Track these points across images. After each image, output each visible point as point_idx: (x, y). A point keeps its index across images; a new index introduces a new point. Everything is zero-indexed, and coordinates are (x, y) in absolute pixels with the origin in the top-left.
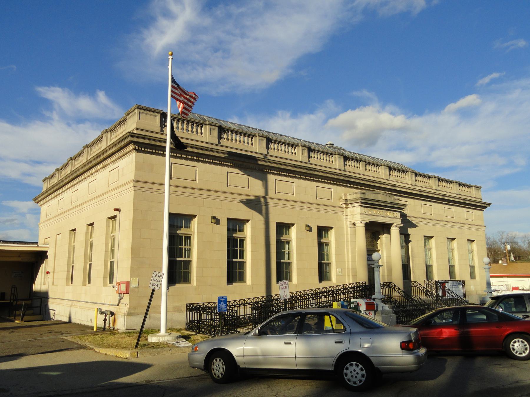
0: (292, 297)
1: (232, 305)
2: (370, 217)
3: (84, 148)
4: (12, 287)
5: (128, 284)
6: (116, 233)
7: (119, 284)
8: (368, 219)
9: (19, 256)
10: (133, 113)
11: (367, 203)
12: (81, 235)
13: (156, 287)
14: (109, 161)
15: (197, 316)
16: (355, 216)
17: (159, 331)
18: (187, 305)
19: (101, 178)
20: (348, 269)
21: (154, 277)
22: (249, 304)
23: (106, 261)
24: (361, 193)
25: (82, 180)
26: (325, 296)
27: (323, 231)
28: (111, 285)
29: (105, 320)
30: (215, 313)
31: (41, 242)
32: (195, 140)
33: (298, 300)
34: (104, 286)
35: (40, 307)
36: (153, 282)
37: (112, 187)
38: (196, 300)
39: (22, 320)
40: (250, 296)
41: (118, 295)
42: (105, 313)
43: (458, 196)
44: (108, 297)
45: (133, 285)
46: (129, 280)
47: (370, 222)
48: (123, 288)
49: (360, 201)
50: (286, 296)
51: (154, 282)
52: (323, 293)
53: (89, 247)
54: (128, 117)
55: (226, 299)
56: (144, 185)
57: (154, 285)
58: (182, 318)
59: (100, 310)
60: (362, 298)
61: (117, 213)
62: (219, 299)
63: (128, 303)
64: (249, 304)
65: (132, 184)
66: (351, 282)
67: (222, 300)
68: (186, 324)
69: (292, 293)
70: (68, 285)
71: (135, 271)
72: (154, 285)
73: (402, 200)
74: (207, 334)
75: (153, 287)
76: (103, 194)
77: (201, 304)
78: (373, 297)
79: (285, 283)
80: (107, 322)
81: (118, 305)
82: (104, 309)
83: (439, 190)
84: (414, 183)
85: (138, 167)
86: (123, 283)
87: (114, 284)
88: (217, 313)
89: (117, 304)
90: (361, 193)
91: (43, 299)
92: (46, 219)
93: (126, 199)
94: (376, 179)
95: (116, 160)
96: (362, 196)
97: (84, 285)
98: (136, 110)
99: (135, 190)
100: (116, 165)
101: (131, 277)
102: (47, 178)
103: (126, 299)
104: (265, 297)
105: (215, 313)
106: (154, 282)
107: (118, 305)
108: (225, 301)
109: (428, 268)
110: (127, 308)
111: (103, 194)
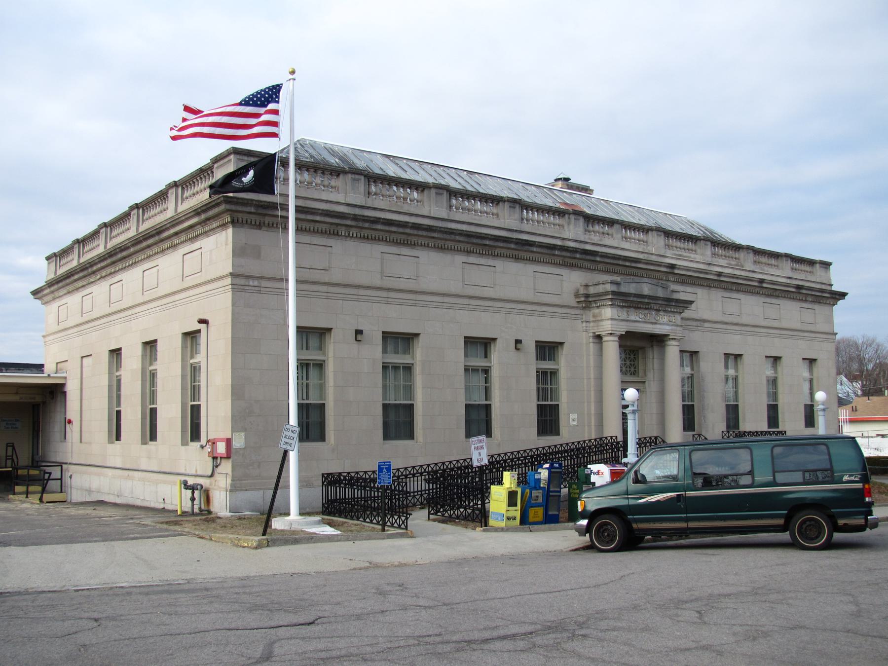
0: (491, 463)
1: (402, 475)
2: (628, 323)
3: (132, 208)
4: (7, 446)
5: (229, 442)
6: (200, 358)
7: (214, 443)
8: (623, 328)
9: (17, 393)
10: (226, 160)
11: (625, 301)
12: (132, 361)
13: (289, 448)
14: (183, 237)
15: (338, 492)
16: (601, 323)
17: (288, 514)
18: (323, 475)
19: (167, 268)
20: (589, 414)
21: (286, 433)
22: (421, 474)
23: (184, 405)
24: (612, 283)
25: (130, 265)
26: (565, 458)
27: (547, 350)
28: (196, 445)
29: (193, 499)
30: (371, 488)
31: (49, 368)
32: (327, 201)
33: (502, 467)
34: (182, 445)
35: (61, 479)
36: (284, 440)
37: (189, 282)
38: (335, 468)
39: (41, 500)
40: (422, 461)
41: (211, 459)
42: (193, 488)
43: (788, 281)
44: (194, 460)
45: (239, 442)
46: (230, 437)
47: (627, 332)
48: (221, 448)
49: (610, 297)
50: (482, 460)
51: (287, 440)
52: (561, 452)
53: (150, 379)
54: (216, 166)
55: (390, 466)
56: (251, 283)
57: (286, 443)
58: (317, 494)
59: (185, 483)
60: (606, 463)
61: (203, 327)
62: (379, 466)
63: (230, 473)
64: (421, 474)
65: (228, 281)
66: (593, 437)
67: (384, 467)
68: (323, 505)
69: (492, 456)
70: (113, 443)
71: (239, 419)
72: (286, 443)
73: (684, 293)
74: (358, 519)
75: (285, 447)
76: (174, 293)
77: (353, 475)
78: (624, 460)
79: (481, 441)
80: (196, 502)
81: (212, 476)
82: (191, 481)
83: (753, 272)
84: (709, 259)
85: (238, 252)
86: (221, 440)
87: (203, 441)
88: (374, 487)
89: (210, 473)
90: (612, 283)
91: (64, 466)
92: (57, 328)
93: (219, 306)
94: (641, 256)
95: (197, 236)
96: (614, 288)
97: (144, 442)
98: (232, 157)
99: (233, 290)
100: (196, 245)
101: (233, 431)
102: (55, 255)
103: (226, 467)
104: (636, 403)
105: (371, 488)
106: (287, 440)
107: (212, 476)
108: (389, 469)
109: (733, 413)
110: (229, 481)
111: (174, 293)
